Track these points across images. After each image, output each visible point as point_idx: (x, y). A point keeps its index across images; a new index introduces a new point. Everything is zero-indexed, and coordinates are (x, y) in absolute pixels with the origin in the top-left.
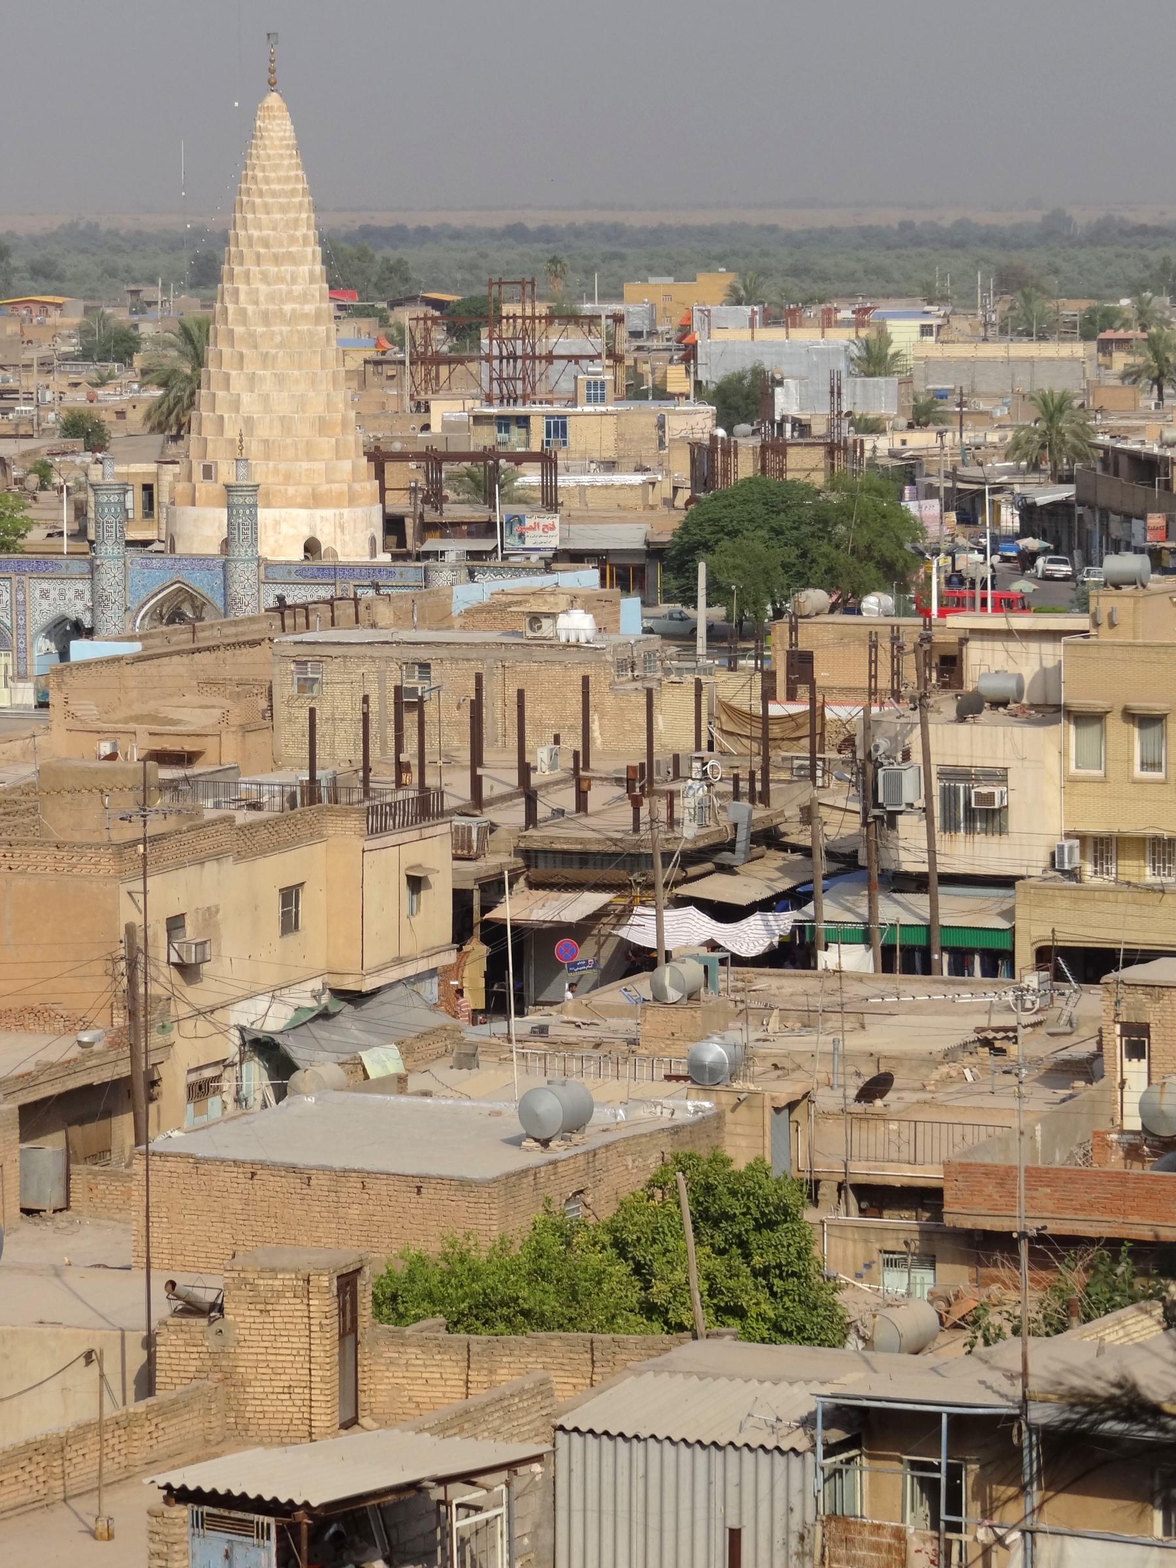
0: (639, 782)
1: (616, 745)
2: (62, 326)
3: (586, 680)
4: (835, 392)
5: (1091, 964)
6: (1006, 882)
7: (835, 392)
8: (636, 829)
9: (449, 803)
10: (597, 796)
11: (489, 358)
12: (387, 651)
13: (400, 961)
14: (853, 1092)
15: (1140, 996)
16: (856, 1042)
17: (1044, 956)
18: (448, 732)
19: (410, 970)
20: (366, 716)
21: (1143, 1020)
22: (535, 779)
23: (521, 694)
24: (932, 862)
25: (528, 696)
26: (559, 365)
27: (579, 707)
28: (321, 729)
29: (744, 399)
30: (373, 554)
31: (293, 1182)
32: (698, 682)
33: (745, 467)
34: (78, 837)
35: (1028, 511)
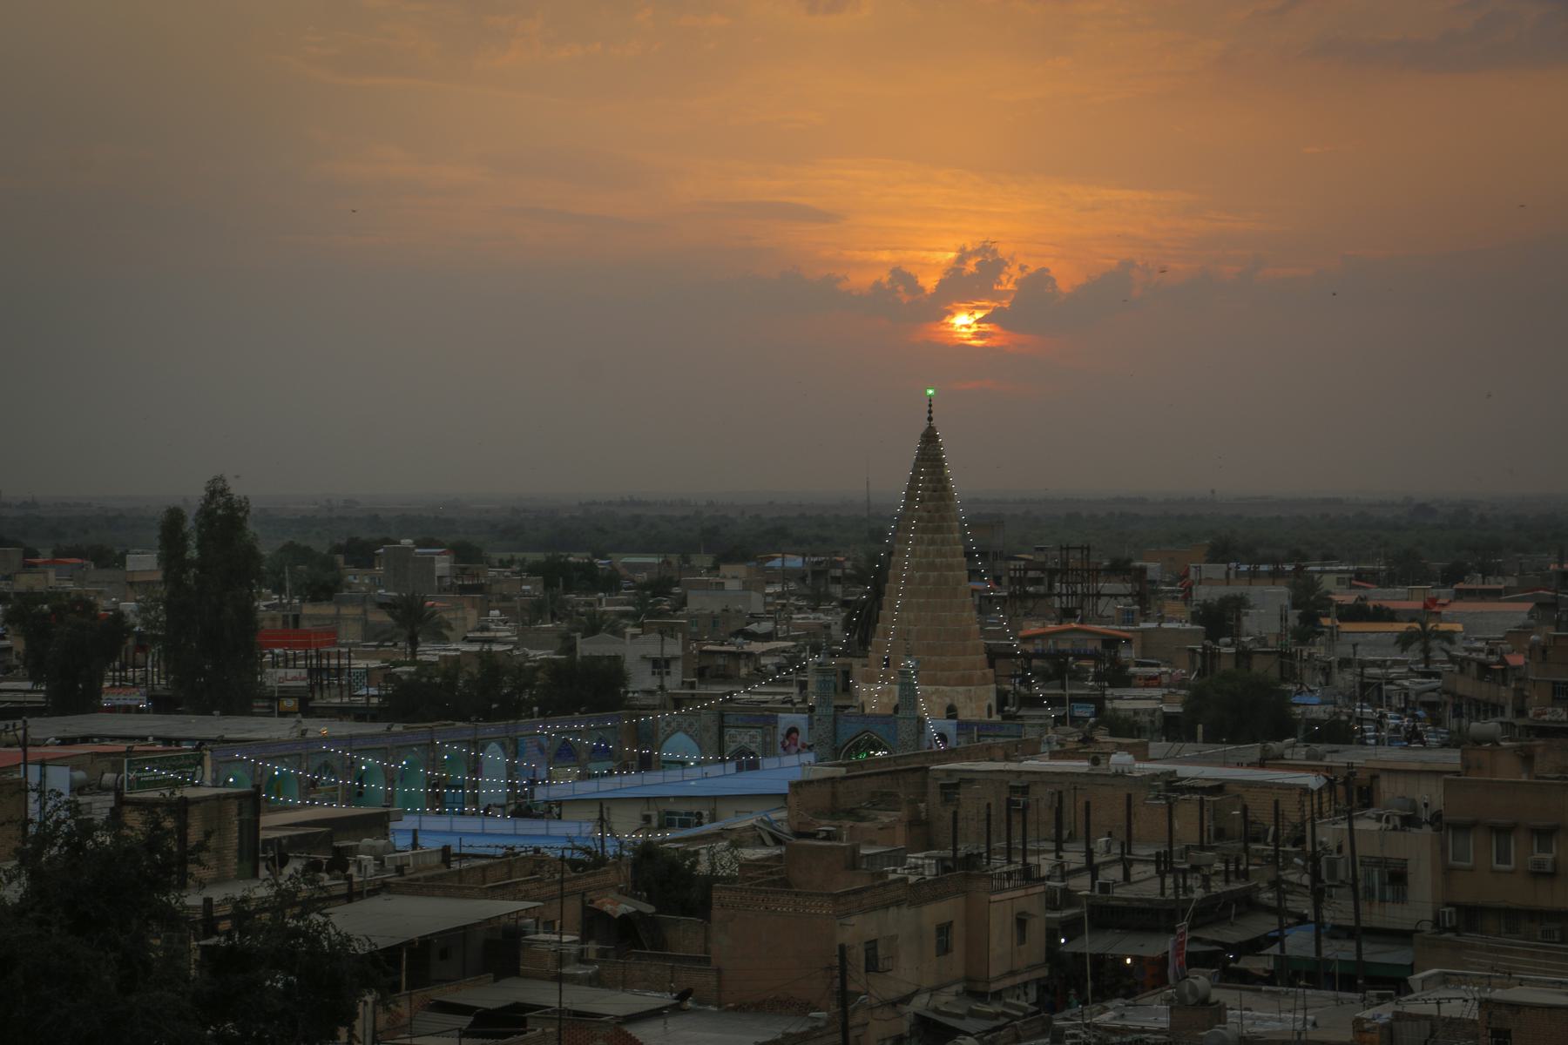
2: (578, 604)
3: (1129, 796)
8: (1163, 894)
10: (1137, 871)
11: (1060, 595)
13: (1012, 973)
19: (1018, 980)
20: (989, 815)
22: (1097, 859)
23: (1088, 804)
26: (1103, 601)
28: (960, 824)
29: (1219, 619)
30: (990, 715)
32: (1202, 801)
33: (1227, 665)
35: (1011, 579)
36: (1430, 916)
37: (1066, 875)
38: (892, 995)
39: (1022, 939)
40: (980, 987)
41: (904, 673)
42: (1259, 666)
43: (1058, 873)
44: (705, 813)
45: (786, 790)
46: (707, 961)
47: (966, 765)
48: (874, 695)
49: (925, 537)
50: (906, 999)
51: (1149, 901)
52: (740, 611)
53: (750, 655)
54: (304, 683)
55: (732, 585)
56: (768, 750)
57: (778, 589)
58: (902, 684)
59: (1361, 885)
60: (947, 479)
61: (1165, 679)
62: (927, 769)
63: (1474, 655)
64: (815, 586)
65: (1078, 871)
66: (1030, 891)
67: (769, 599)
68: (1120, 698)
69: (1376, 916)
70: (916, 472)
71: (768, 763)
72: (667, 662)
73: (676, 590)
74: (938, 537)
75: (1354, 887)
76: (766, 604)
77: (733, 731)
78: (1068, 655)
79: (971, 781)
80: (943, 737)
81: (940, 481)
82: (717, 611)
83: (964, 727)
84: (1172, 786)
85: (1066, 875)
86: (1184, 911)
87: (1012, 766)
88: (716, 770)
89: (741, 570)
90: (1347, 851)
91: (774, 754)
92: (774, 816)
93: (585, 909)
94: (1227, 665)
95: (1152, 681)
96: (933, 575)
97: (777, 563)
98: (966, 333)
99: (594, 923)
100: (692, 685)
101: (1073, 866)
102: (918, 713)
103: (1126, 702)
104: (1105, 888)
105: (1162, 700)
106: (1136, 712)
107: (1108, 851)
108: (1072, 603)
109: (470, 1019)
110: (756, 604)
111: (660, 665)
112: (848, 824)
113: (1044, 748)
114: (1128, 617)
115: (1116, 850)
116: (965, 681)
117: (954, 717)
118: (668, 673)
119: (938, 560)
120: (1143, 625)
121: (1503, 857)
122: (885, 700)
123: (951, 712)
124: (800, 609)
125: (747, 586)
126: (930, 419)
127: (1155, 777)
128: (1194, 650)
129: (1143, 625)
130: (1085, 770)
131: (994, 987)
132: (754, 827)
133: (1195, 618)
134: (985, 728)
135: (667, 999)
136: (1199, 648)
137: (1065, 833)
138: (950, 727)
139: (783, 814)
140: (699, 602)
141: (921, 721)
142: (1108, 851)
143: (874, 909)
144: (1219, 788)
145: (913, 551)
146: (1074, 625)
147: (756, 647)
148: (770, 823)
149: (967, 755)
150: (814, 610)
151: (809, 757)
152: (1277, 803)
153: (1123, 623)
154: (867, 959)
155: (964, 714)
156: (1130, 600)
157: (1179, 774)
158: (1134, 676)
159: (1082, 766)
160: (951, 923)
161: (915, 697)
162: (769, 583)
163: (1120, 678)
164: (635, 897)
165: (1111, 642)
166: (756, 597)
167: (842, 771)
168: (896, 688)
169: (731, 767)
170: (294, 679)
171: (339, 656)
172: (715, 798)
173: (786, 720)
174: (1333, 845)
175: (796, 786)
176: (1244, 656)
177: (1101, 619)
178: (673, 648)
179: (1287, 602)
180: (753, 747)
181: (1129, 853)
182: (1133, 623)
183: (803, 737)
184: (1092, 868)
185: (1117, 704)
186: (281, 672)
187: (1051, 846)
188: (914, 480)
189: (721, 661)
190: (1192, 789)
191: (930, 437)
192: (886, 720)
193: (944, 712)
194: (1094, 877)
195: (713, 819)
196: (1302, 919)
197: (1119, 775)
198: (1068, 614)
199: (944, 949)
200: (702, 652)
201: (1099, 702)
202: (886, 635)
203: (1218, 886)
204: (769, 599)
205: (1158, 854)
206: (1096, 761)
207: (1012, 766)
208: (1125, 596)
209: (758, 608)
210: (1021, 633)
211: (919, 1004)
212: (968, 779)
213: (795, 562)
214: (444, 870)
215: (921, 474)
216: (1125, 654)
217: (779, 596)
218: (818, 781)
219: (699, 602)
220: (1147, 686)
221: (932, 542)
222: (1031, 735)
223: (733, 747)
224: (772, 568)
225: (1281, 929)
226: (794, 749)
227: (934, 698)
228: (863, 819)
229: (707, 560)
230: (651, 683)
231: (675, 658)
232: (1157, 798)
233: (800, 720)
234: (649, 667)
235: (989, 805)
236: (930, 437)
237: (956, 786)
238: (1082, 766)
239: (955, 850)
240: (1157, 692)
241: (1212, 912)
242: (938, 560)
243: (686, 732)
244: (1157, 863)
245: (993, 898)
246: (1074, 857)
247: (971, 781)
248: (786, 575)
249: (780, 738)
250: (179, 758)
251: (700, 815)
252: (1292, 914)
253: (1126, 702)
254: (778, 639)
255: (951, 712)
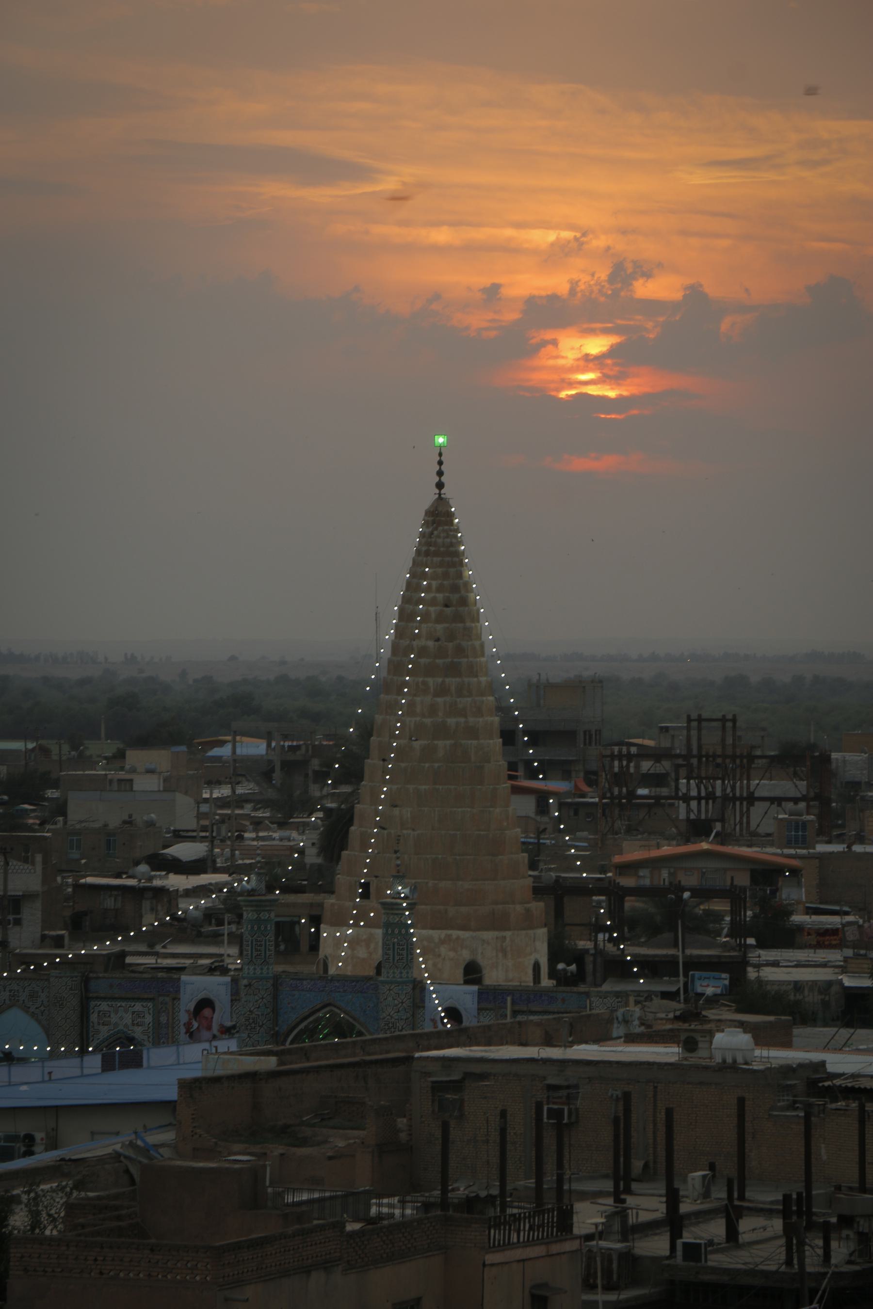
3: (741, 1101)
10: (746, 1225)
11: (687, 799)
22: (685, 1208)
23: (669, 1113)
37: (629, 1231)
41: (392, 907)
43: (617, 1226)
44: (39, 1136)
45: (172, 1094)
47: (477, 1051)
48: (345, 945)
49: (430, 681)
51: (766, 1274)
52: (151, 824)
55: (145, 784)
56: (162, 1035)
57: (224, 791)
58: (387, 925)
60: (467, 585)
61: (851, 935)
62: (409, 1059)
64: (286, 785)
65: (650, 1227)
66: (555, 1248)
67: (204, 808)
68: (775, 964)
70: (416, 574)
71: (155, 1056)
73: (51, 793)
74: (452, 682)
76: (200, 816)
77: (104, 1006)
78: (684, 889)
79: (482, 1076)
80: (453, 1013)
81: (455, 589)
82: (114, 822)
83: (491, 997)
84: (816, 1084)
85: (629, 1231)
86: (813, 1292)
87: (554, 1053)
88: (67, 1067)
89: (160, 758)
91: (174, 1041)
92: (153, 1138)
95: (826, 938)
96: (443, 745)
97: (225, 751)
98: (591, 384)
101: (645, 1217)
102: (415, 974)
103: (779, 969)
104: (693, 1251)
105: (844, 970)
106: (798, 986)
107: (706, 1195)
108: (707, 810)
110: (184, 812)
112: (278, 1150)
113: (618, 1030)
114: (796, 834)
115: (720, 1193)
116: (498, 922)
117: (478, 981)
118: (18, 922)
119: (451, 721)
120: (821, 848)
122: (362, 953)
123: (472, 973)
124: (257, 824)
125: (170, 785)
126: (440, 485)
127: (787, 1070)
129: (821, 848)
130: (673, 1059)
132: (117, 1156)
134: (525, 998)
137: (637, 1165)
138: (466, 997)
139: (169, 1136)
140: (88, 810)
141: (419, 987)
142: (706, 1195)
145: (411, 704)
146: (705, 846)
147: (176, 882)
148: (145, 1151)
149: (488, 1037)
150: (282, 825)
151: (232, 1045)
153: (789, 844)
155: (493, 977)
157: (830, 1068)
158: (800, 928)
159: (668, 1053)
160: (418, 1300)
161: (411, 947)
162: (212, 783)
163: (778, 933)
165: (766, 875)
166: (183, 802)
167: (270, 1063)
168: (379, 932)
169: (94, 1062)
172: (57, 1110)
173: (195, 986)
175: (189, 1087)
177: (753, 838)
180: (138, 1032)
181: (742, 1197)
182: (803, 842)
183: (222, 1016)
184: (674, 1222)
185: (770, 974)
187: (608, 1185)
188: (412, 587)
189: (110, 903)
191: (439, 516)
192: (359, 984)
193: (459, 974)
194: (676, 1235)
195: (53, 1144)
197: (729, 1067)
198: (698, 829)
200: (77, 887)
201: (736, 968)
202: (365, 845)
204: (204, 808)
205: (787, 1198)
206: (690, 1045)
207: (554, 1053)
208: (796, 800)
209: (187, 820)
210: (617, 859)
212: (476, 1073)
213: (254, 748)
215: (424, 576)
216: (789, 893)
217: (223, 803)
218: (231, 1078)
219: (88, 810)
220: (819, 946)
221: (442, 691)
222: (599, 1008)
223: (104, 1032)
224: (218, 759)
226: (206, 1034)
227: (443, 950)
228: (303, 1142)
229: (109, 748)
231: (29, 897)
232: (792, 1106)
233: (216, 987)
235: (503, 1114)
236: (439, 516)
237: (457, 1086)
238: (668, 1053)
239: (445, 1191)
240: (835, 956)
242: (451, 721)
243: (26, 1009)
244: (786, 1214)
245: (490, 1258)
246: (647, 1205)
247: (482, 1076)
248: (239, 769)
249: (183, 1017)
251: (29, 1139)
253: (779, 969)
254: (216, 870)
255: (472, 973)
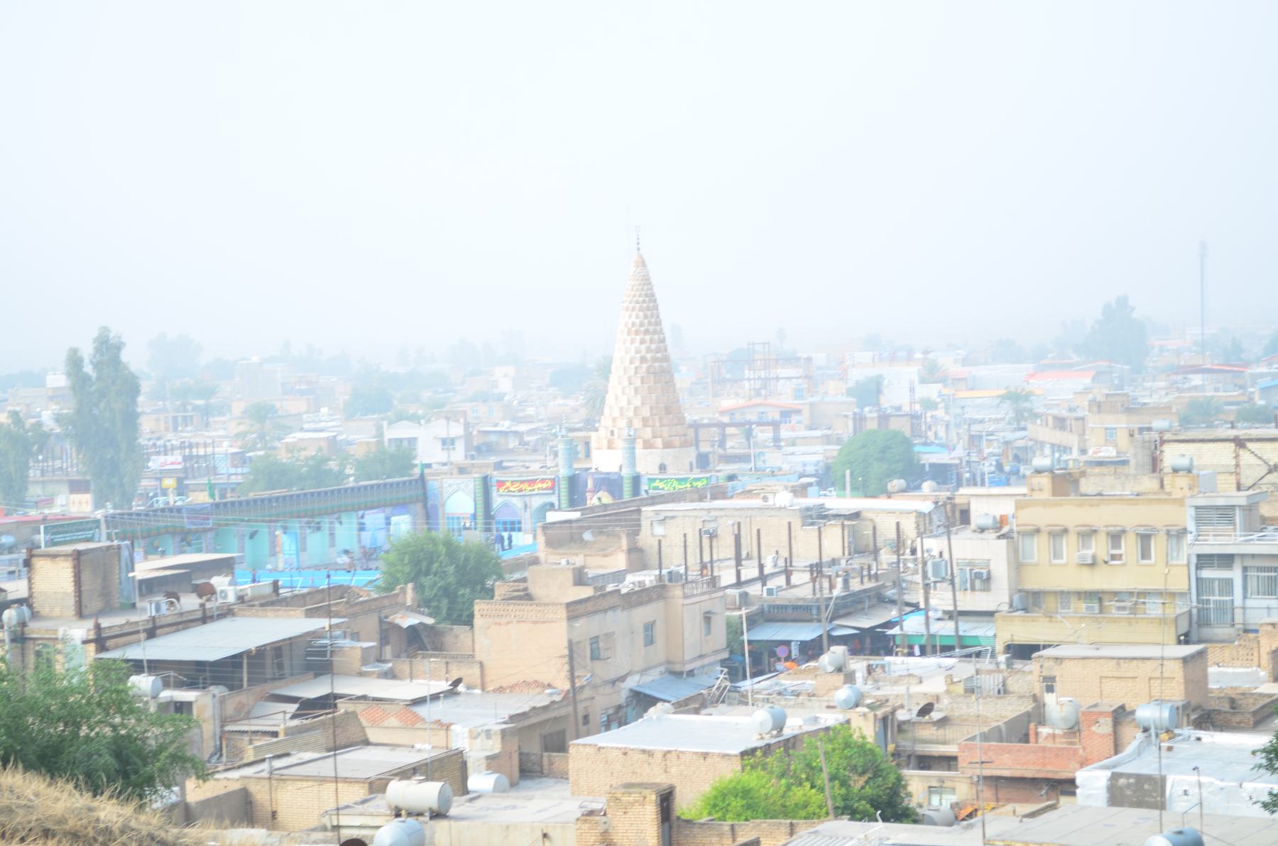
0: (816, 570)
1: (806, 553)
4: (912, 390)
5: (1023, 652)
6: (990, 614)
7: (912, 390)
8: (814, 594)
9: (723, 583)
10: (795, 579)
11: (749, 379)
12: (695, 513)
13: (701, 656)
14: (915, 712)
15: (1051, 663)
16: (916, 689)
17: (1009, 648)
18: (725, 549)
19: (706, 661)
21: (1053, 674)
22: (767, 571)
24: (955, 606)
25: (663, 544)
26: (782, 382)
27: (786, 538)
31: (644, 757)
33: (872, 425)
34: (666, 488)
36: (1007, 599)
38: (613, 676)
39: (708, 632)
40: (678, 668)
42: (894, 425)
46: (473, 656)
50: (622, 679)
53: (516, 433)
54: (180, 467)
59: (957, 580)
63: (1050, 411)
68: (793, 454)
69: (970, 601)
72: (453, 441)
75: (952, 583)
90: (946, 556)
93: (381, 621)
94: (872, 425)
99: (387, 632)
100: (472, 457)
104: (770, 592)
109: (296, 706)
111: (448, 443)
121: (1057, 555)
128: (846, 416)
131: (688, 667)
133: (850, 392)
135: (444, 686)
136: (850, 414)
143: (595, 612)
144: (856, 515)
152: (898, 524)
154: (592, 651)
156: (800, 381)
164: (419, 612)
170: (172, 463)
171: (205, 445)
174: (935, 553)
176: (884, 418)
178: (457, 430)
179: (916, 378)
186: (162, 459)
190: (837, 516)
196: (916, 607)
199: (650, 641)
203: (856, 585)
206: (765, 499)
211: (632, 683)
214: (275, 598)
225: (901, 616)
230: (441, 456)
234: (439, 445)
241: (851, 604)
250: (62, 526)
252: (908, 604)
